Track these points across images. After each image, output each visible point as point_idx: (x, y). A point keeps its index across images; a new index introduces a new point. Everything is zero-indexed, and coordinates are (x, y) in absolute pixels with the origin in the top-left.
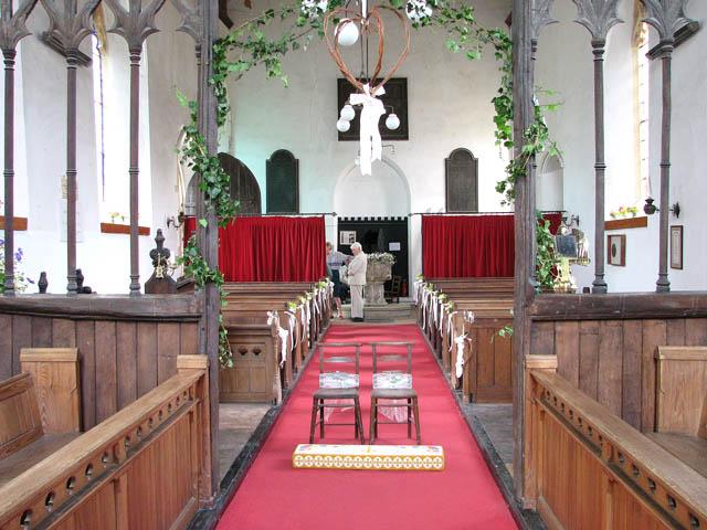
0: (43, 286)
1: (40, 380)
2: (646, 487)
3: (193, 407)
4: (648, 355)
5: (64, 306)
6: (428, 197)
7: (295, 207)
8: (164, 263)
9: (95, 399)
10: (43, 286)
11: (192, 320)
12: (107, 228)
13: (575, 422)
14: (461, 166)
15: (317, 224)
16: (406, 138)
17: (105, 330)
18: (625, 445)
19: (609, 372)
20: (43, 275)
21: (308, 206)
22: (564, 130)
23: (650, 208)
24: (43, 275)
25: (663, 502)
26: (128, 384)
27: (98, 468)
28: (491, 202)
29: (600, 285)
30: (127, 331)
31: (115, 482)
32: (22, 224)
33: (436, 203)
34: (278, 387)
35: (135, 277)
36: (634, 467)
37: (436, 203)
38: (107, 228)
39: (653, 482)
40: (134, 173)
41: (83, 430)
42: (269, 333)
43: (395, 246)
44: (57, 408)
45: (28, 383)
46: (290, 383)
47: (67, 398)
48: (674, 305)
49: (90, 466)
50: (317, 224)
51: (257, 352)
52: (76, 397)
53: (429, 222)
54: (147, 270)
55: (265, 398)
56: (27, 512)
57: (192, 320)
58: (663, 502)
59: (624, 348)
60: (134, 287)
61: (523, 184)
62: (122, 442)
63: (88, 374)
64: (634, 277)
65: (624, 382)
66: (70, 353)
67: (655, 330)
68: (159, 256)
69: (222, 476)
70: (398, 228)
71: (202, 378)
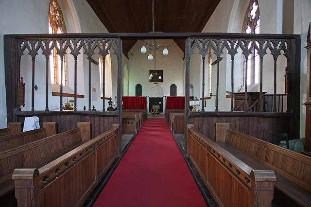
0: (85, 109)
1: (82, 129)
2: (217, 156)
3: (116, 135)
4: (214, 125)
5: (88, 113)
6: (167, 94)
7: (141, 95)
8: (111, 104)
9: (94, 133)
10: (85, 109)
11: (117, 116)
12: (83, 97)
13: (203, 144)
14: (173, 88)
15: (145, 98)
16: (163, 82)
17: (97, 118)
18: (211, 146)
19: (205, 128)
20: (85, 107)
21: (143, 95)
22: (195, 81)
23: (211, 95)
24: (85, 107)
25: (228, 165)
26: (102, 129)
27: (90, 150)
28: (180, 93)
29: (203, 110)
30: (102, 118)
31: (94, 153)
32: (102, 98)
33: (169, 95)
34: (136, 130)
35: (104, 107)
36: (223, 159)
37: (169, 95)
38: (83, 97)
39: (219, 155)
40: (104, 84)
41: (91, 139)
42: (134, 119)
43: (160, 103)
44: (85, 135)
45: (79, 130)
46: (138, 129)
47: (88, 133)
48: (219, 114)
49: (81, 154)
50: (145, 98)
51: (132, 123)
52: (90, 133)
53: (168, 98)
54: (106, 107)
55: (133, 132)
56: (67, 163)
57: (117, 116)
58: (222, 160)
59: (208, 123)
60: (104, 109)
61: (210, 69)
62: (96, 144)
63: (93, 129)
64: (210, 108)
65: (208, 130)
66: (89, 123)
67: (215, 120)
68: (110, 103)
69: (122, 149)
70: (161, 99)
71: (118, 129)
